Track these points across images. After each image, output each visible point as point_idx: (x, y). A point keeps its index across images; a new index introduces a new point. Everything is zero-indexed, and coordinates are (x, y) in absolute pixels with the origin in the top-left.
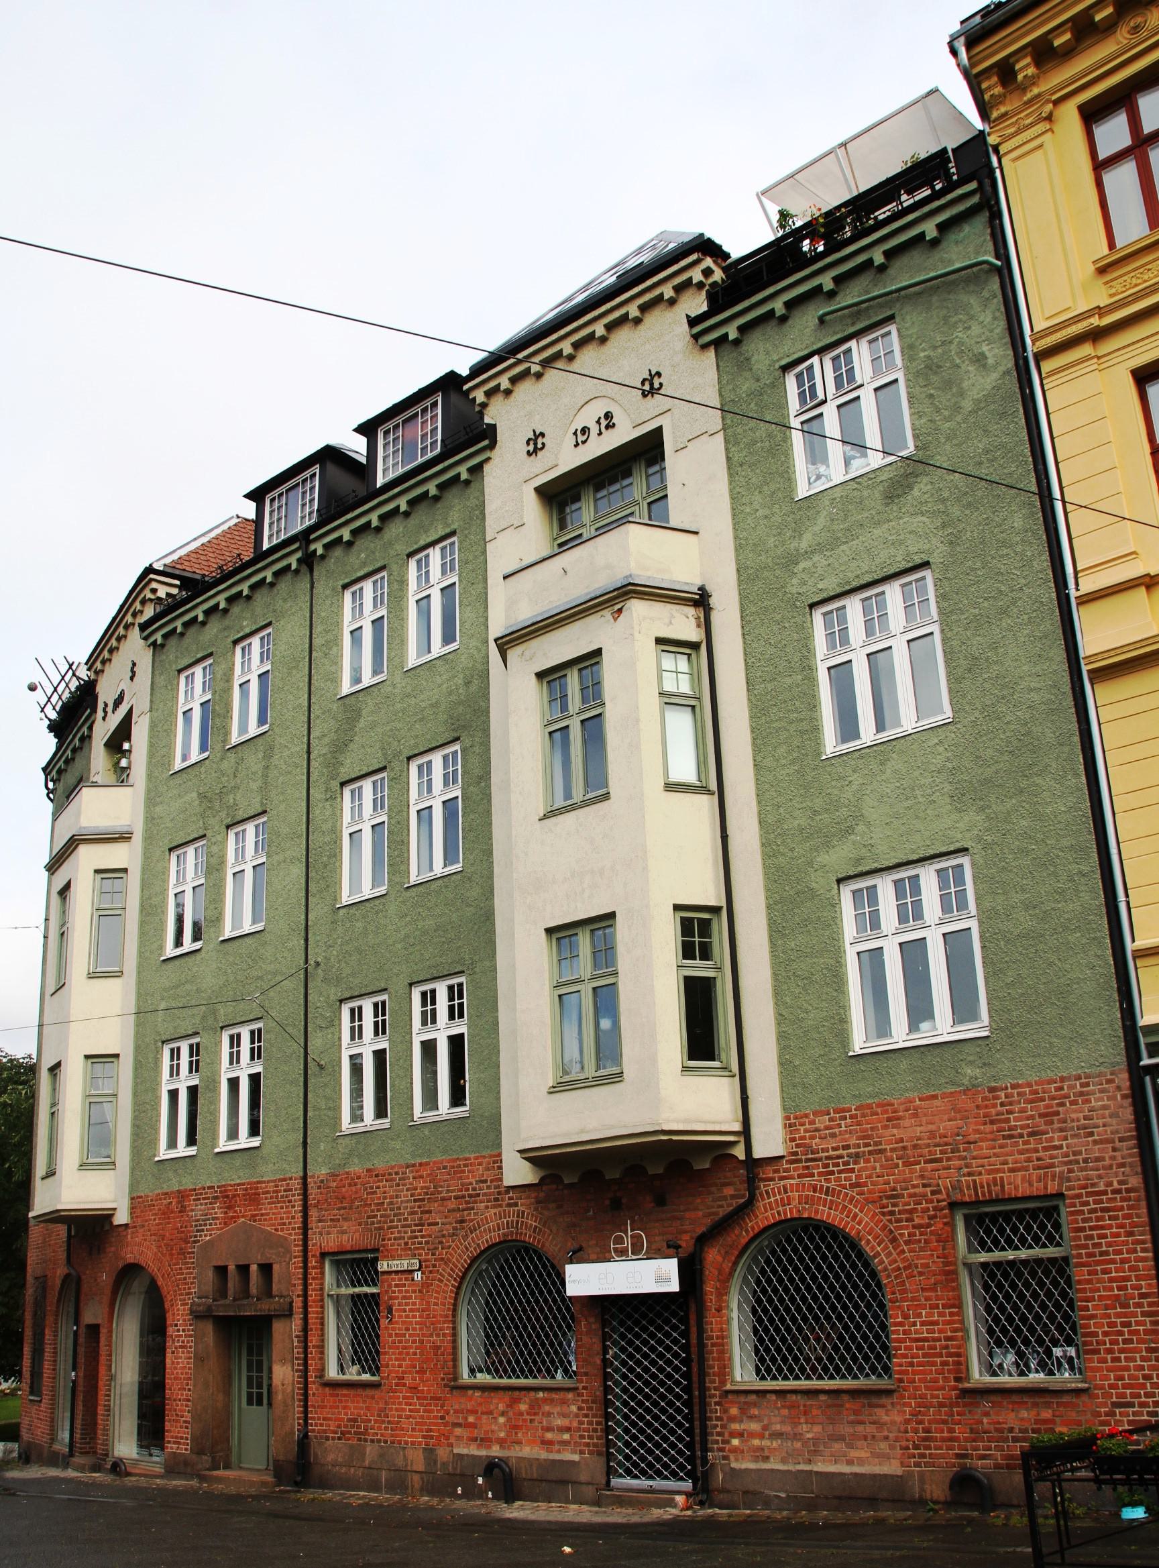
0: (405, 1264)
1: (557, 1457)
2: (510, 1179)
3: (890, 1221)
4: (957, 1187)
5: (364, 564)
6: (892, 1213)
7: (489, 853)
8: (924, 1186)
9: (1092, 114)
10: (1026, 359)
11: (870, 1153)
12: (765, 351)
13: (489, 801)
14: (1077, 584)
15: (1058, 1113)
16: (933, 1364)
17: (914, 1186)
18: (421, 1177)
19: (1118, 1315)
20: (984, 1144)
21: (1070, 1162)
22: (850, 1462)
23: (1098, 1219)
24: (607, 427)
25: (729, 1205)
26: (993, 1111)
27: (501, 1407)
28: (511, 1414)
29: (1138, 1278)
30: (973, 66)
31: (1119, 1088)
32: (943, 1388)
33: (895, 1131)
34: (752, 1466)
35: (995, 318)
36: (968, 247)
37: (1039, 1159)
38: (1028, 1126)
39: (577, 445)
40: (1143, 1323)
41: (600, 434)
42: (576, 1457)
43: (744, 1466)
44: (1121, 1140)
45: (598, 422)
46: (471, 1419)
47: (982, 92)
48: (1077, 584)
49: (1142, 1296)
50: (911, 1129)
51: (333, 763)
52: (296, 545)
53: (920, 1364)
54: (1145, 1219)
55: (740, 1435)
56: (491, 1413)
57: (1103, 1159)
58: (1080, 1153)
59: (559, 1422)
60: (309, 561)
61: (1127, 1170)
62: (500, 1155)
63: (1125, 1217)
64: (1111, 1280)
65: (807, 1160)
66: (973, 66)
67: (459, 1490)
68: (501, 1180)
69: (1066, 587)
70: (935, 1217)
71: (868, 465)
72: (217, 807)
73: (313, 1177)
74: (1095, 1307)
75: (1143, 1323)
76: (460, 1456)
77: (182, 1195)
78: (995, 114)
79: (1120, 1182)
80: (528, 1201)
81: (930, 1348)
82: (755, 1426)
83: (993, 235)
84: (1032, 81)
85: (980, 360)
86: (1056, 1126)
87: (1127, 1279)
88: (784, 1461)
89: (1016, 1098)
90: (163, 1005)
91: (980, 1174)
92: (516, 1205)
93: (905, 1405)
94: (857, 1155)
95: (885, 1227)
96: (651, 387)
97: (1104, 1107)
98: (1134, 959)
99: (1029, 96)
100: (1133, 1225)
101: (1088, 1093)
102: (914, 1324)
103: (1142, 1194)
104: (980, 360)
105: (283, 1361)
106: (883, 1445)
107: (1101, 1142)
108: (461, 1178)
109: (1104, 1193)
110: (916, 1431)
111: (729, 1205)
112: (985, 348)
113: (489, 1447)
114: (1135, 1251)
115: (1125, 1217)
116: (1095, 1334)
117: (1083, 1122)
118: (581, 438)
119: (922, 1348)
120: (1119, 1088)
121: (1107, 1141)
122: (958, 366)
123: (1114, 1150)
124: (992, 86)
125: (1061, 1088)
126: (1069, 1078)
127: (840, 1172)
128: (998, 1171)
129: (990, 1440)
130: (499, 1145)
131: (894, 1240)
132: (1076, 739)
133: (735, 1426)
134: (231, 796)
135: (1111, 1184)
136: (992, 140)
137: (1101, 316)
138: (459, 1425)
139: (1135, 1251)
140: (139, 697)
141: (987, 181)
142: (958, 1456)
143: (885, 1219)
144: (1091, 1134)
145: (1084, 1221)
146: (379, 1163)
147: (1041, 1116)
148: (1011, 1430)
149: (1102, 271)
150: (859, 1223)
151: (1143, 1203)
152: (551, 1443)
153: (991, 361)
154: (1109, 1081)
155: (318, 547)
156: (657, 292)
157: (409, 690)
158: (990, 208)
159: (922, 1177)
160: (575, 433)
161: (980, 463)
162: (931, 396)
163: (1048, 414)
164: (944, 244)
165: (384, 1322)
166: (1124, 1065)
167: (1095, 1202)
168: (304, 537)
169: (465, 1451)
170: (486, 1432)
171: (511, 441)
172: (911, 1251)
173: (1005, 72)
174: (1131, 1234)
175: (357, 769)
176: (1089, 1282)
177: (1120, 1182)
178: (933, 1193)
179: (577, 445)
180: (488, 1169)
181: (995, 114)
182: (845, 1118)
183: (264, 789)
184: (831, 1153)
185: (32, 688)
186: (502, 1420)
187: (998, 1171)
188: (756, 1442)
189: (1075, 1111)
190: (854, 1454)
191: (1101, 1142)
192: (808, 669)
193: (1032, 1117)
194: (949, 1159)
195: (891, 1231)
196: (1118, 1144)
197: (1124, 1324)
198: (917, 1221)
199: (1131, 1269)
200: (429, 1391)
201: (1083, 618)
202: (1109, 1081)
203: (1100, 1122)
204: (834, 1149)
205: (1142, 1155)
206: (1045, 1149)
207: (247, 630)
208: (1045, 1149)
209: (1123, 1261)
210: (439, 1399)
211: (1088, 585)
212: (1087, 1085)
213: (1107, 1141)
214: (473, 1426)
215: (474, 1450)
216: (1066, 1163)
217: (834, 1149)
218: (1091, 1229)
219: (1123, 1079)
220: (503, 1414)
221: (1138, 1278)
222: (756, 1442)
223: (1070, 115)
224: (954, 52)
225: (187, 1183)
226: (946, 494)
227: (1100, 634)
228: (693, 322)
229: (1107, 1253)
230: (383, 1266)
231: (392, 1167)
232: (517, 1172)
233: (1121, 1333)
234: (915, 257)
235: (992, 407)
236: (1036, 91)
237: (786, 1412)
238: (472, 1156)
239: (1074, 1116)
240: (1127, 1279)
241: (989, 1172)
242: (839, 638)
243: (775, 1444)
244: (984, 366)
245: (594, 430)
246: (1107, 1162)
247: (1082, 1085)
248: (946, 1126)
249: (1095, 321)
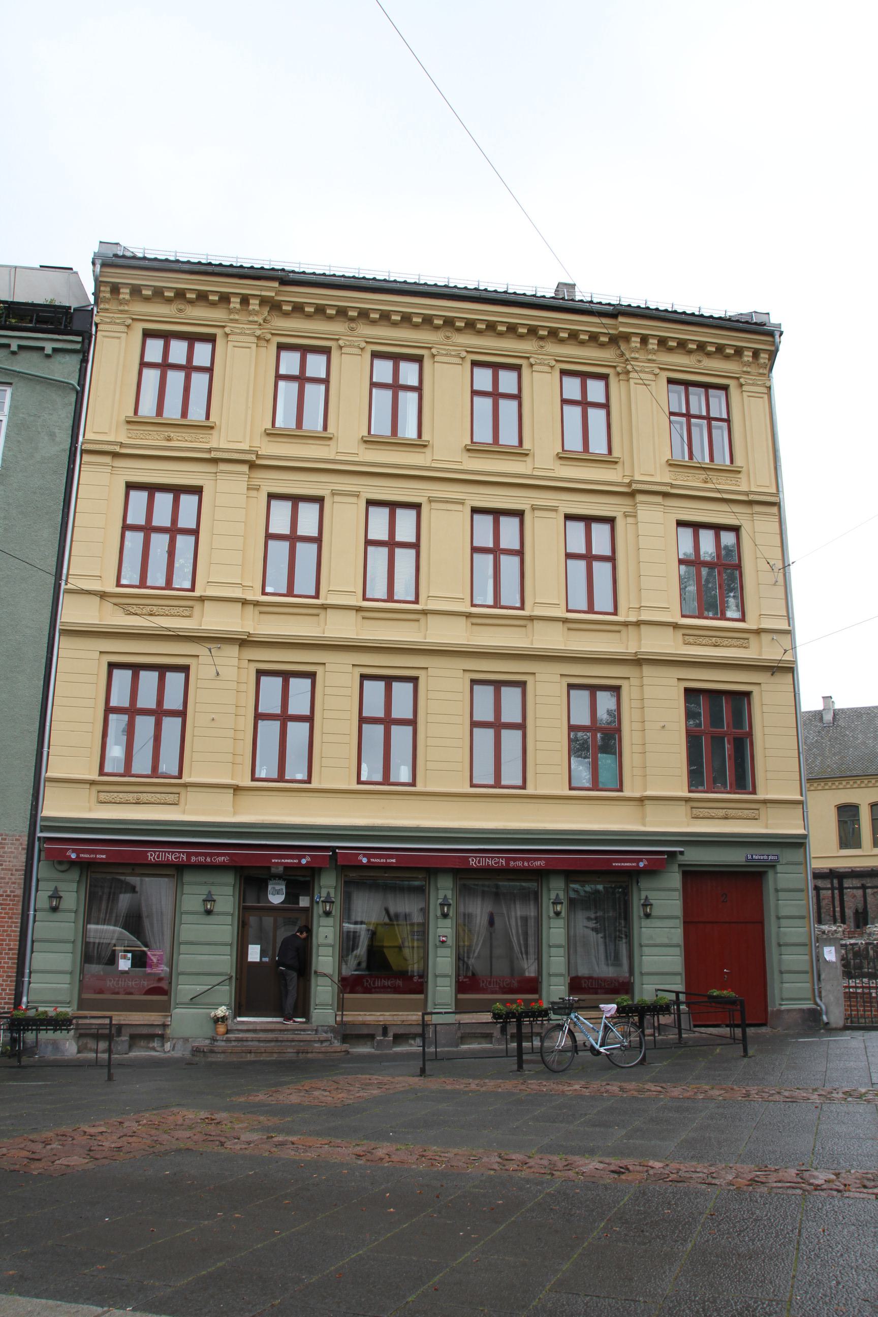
9: (148, 334)
10: (76, 448)
14: (67, 581)
30: (101, 276)
31: (21, 844)
35: (67, 417)
40: (7, 963)
44: (17, 870)
47: (100, 291)
49: (10, 949)
54: (20, 911)
61: (16, 886)
63: (10, 909)
66: (101, 276)
69: (61, 579)
71: (175, 784)
75: (7, 963)
78: (102, 306)
79: (11, 892)
83: (80, 370)
84: (126, 302)
85: (52, 435)
97: (12, 852)
98: (45, 781)
99: (121, 308)
100: (13, 914)
103: (21, 899)
107: (6, 869)
112: (57, 431)
114: (11, 927)
115: (10, 909)
120: (21, 844)
121: (9, 870)
122: (39, 433)
123: (12, 875)
124: (106, 293)
132: (44, 661)
135: (6, 892)
136: (96, 319)
137: (121, 447)
141: (87, 341)
149: (128, 422)
151: (21, 904)
153: (58, 439)
154: (17, 840)
158: (84, 353)
161: (35, 493)
162: (19, 441)
163: (78, 484)
164: (52, 360)
166: (27, 833)
173: (115, 289)
174: (11, 918)
177: (11, 892)
181: (102, 306)
191: (6, 869)
196: (14, 872)
199: (7, 935)
201: (66, 601)
202: (17, 840)
203: (8, 859)
205: (25, 879)
212: (5, 839)
213: (9, 870)
219: (25, 840)
221: (9, 940)
223: (139, 328)
224: (94, 263)
226: (11, 501)
227: (73, 612)
234: (35, 356)
235: (50, 465)
236: (126, 308)
244: (53, 440)
246: (7, 880)
249: (117, 449)
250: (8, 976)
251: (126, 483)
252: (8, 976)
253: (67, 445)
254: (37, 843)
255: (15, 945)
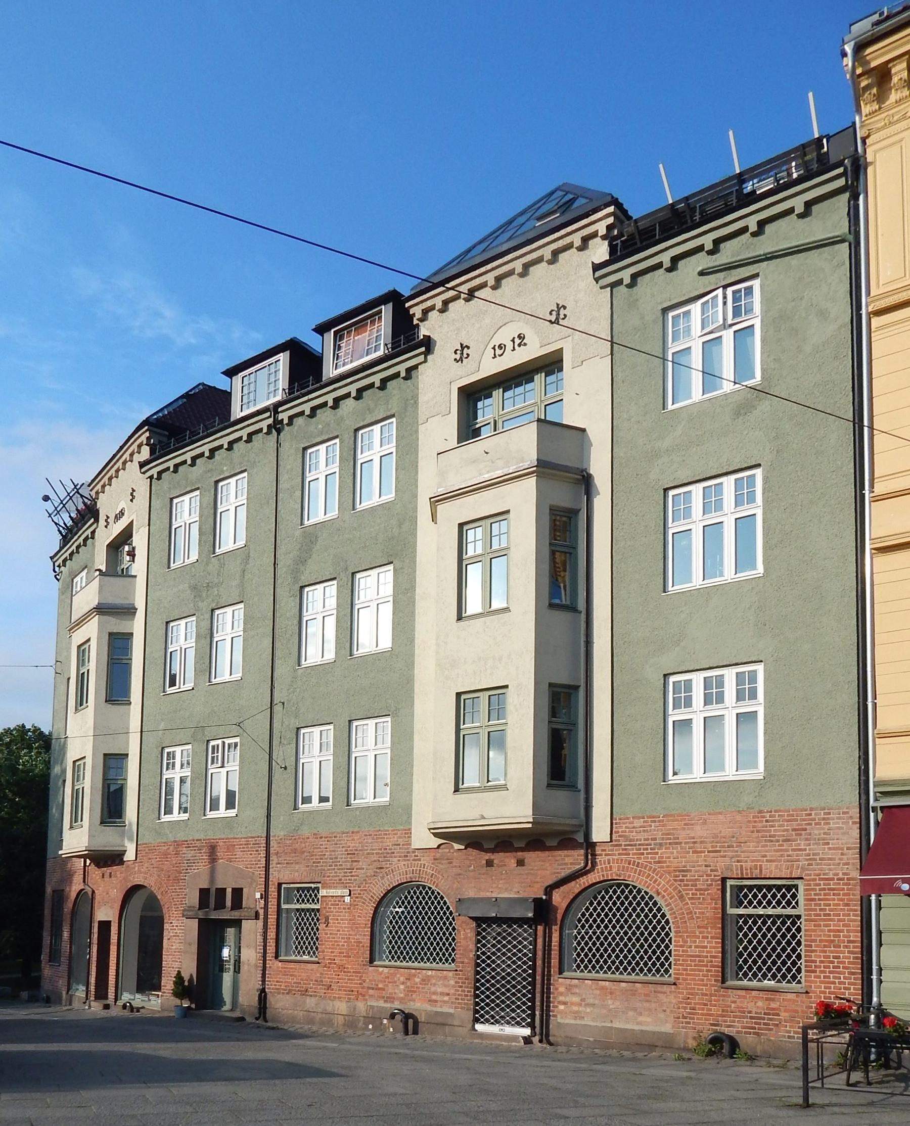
0: (339, 892)
1: (439, 1010)
2: (416, 843)
3: (680, 885)
4: (729, 868)
5: (321, 433)
6: (682, 881)
7: (412, 640)
8: (706, 866)
11: (670, 843)
12: (657, 289)
13: (414, 605)
15: (805, 830)
16: (700, 971)
17: (699, 866)
18: (353, 840)
19: (832, 952)
20: (752, 844)
21: (810, 859)
22: (638, 1023)
23: (825, 895)
24: (519, 345)
25: (569, 869)
26: (760, 825)
27: (402, 979)
28: (408, 984)
29: (848, 931)
31: (851, 817)
32: (706, 985)
33: (688, 832)
34: (572, 1022)
36: (832, 219)
37: (788, 856)
38: (783, 836)
39: (495, 357)
41: (514, 349)
42: (452, 1011)
43: (567, 1021)
45: (513, 341)
46: (380, 986)
48: (872, 486)
49: (849, 942)
50: (699, 831)
51: (295, 573)
52: (268, 414)
53: (691, 970)
55: (565, 1003)
56: (395, 982)
57: (834, 859)
58: (818, 854)
59: (439, 990)
60: (277, 427)
62: (410, 829)
64: (829, 931)
65: (625, 845)
67: (370, 1026)
68: (410, 844)
70: (711, 885)
72: (204, 595)
73: (274, 836)
74: (817, 946)
76: (372, 1007)
77: (178, 844)
79: (843, 874)
80: (428, 858)
81: (700, 961)
82: (576, 999)
85: (823, 314)
86: (803, 837)
87: (842, 931)
88: (593, 1020)
89: (777, 818)
90: (162, 726)
91: (746, 862)
92: (420, 860)
93: (679, 993)
94: (661, 844)
95: (676, 888)
96: (558, 316)
97: (839, 828)
101: (828, 819)
102: (691, 947)
104: (823, 314)
105: (248, 946)
106: (662, 1015)
107: (834, 849)
108: (382, 842)
109: (833, 879)
110: (685, 1008)
111: (569, 869)
113: (393, 1002)
114: (849, 915)
116: (815, 962)
117: (822, 836)
118: (498, 352)
119: (695, 961)
125: (810, 815)
126: (816, 809)
127: (647, 854)
128: (758, 861)
129: (735, 1017)
130: (410, 823)
131: (681, 897)
133: (561, 998)
134: (215, 589)
135: (837, 874)
138: (373, 989)
139: (849, 915)
140: (137, 514)
142: (712, 1025)
143: (676, 884)
144: (828, 843)
145: (815, 895)
146: (323, 831)
147: (794, 830)
148: (750, 1012)
150: (658, 885)
152: (436, 1001)
154: (844, 813)
155: (284, 416)
156: (567, 240)
157: (355, 525)
159: (705, 861)
160: (494, 348)
165: (322, 926)
167: (824, 884)
168: (275, 408)
169: (375, 1004)
170: (391, 994)
171: (444, 352)
172: (692, 904)
174: (847, 905)
175: (313, 578)
176: (815, 931)
177: (843, 874)
178: (711, 871)
179: (495, 357)
180: (400, 837)
182: (655, 822)
183: (242, 586)
184: (642, 842)
185: (46, 498)
186: (402, 987)
187: (758, 861)
188: (575, 1008)
189: (818, 829)
190: (641, 1019)
191: (834, 849)
192: (766, 500)
193: (787, 830)
194: (725, 851)
195: (680, 891)
197: (834, 957)
198: (698, 887)
200: (352, 968)
202: (844, 813)
204: (645, 840)
206: (794, 850)
207: (227, 474)
208: (794, 850)
209: (839, 920)
210: (359, 973)
211: (880, 488)
212: (829, 814)
214: (383, 989)
215: (381, 1003)
216: (807, 860)
217: (645, 840)
218: (819, 900)
220: (403, 983)
222: (575, 1008)
225: (181, 836)
227: (882, 522)
228: (596, 267)
229: (829, 915)
230: (323, 892)
231: (333, 833)
232: (422, 839)
233: (833, 962)
237: (598, 992)
238: (390, 829)
239: (816, 832)
240: (842, 931)
241: (753, 861)
242: (712, 504)
243: (588, 1010)
245: (509, 346)
246: (837, 861)
247: (825, 814)
248: (727, 832)
250: (853, 973)
251: (551, 506)
252: (853, 973)
253: (846, 317)
254: (872, 815)
255: (856, 936)
